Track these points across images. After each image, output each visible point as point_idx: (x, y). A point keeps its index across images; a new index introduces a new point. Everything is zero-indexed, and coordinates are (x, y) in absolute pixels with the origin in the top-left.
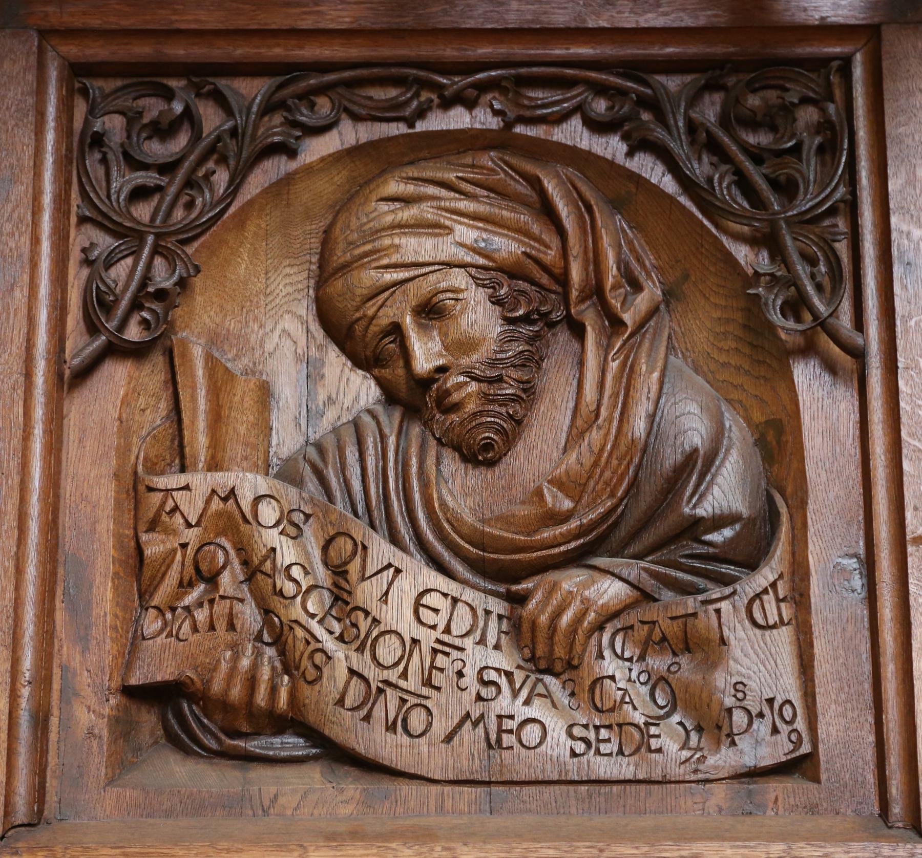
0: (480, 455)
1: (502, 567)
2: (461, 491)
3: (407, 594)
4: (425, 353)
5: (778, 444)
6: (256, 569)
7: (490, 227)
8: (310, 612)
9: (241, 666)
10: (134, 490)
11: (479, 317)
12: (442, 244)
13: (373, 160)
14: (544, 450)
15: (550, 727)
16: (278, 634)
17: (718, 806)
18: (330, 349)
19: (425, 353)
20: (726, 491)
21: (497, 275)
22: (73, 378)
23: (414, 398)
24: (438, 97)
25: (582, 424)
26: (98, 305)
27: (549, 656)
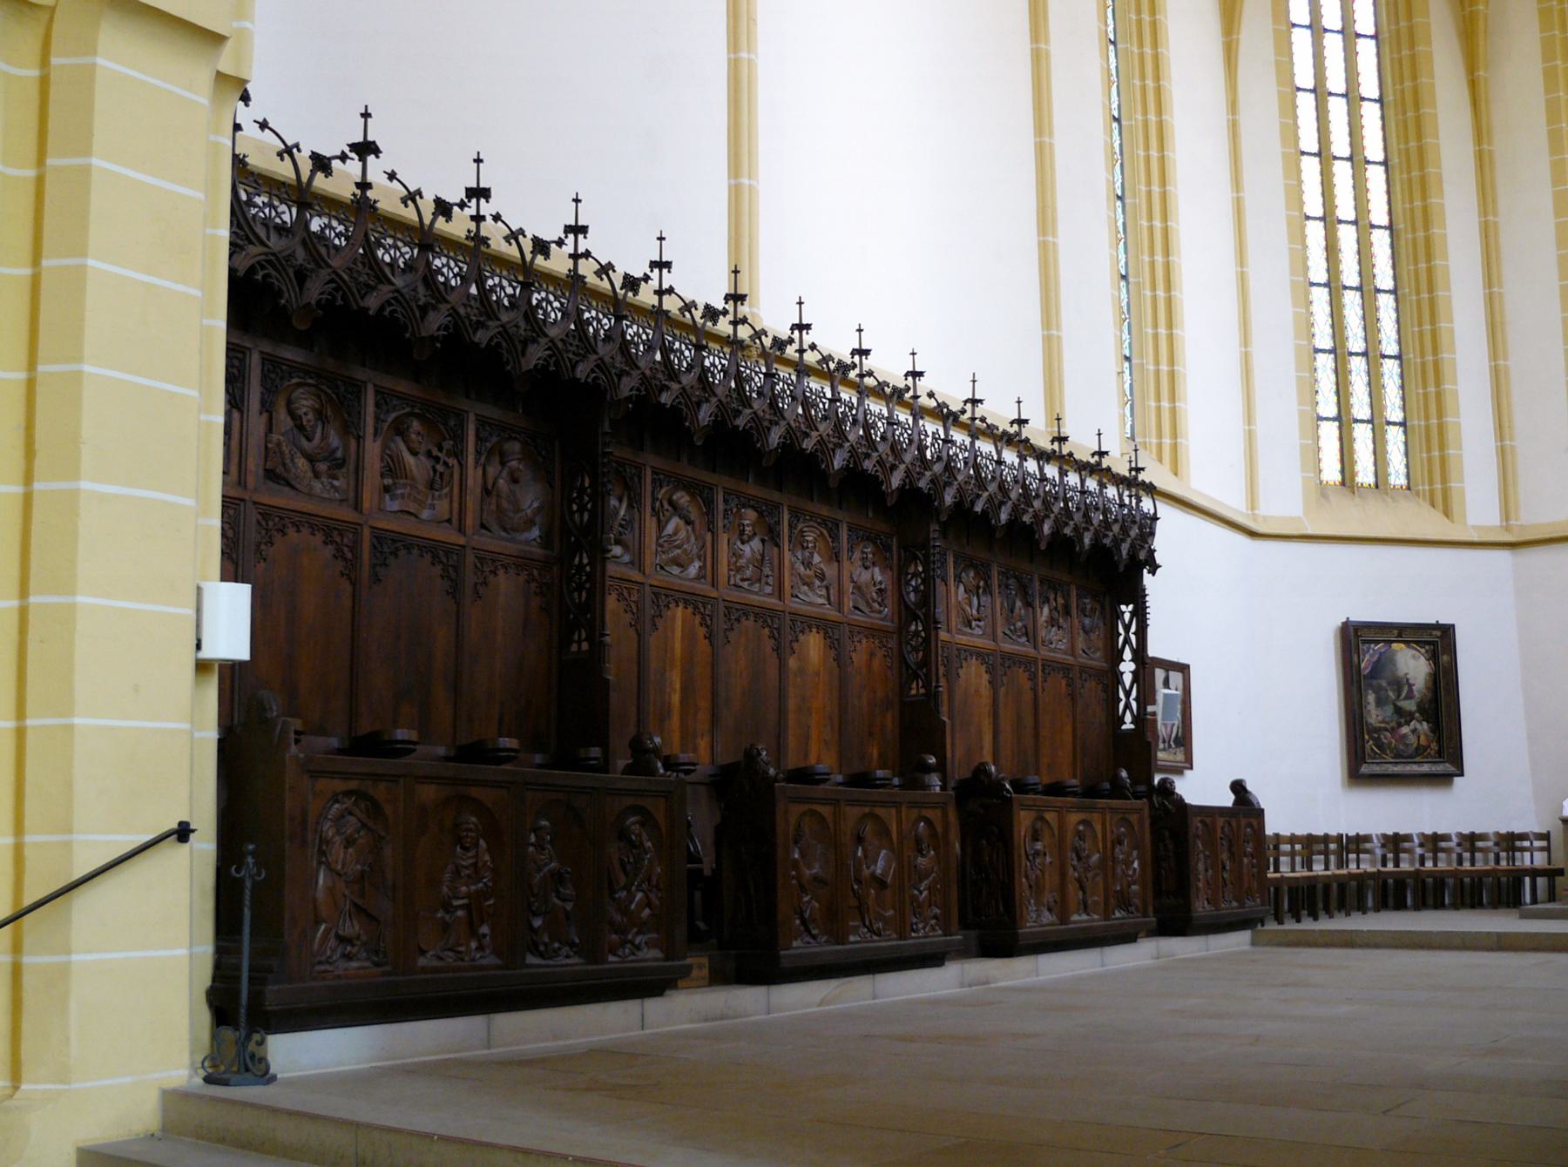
0: (309, 440)
1: (311, 459)
3: (301, 462)
5: (346, 447)
6: (282, 453)
9: (280, 470)
11: (310, 416)
13: (299, 385)
16: (284, 465)
20: (339, 454)
21: (314, 410)
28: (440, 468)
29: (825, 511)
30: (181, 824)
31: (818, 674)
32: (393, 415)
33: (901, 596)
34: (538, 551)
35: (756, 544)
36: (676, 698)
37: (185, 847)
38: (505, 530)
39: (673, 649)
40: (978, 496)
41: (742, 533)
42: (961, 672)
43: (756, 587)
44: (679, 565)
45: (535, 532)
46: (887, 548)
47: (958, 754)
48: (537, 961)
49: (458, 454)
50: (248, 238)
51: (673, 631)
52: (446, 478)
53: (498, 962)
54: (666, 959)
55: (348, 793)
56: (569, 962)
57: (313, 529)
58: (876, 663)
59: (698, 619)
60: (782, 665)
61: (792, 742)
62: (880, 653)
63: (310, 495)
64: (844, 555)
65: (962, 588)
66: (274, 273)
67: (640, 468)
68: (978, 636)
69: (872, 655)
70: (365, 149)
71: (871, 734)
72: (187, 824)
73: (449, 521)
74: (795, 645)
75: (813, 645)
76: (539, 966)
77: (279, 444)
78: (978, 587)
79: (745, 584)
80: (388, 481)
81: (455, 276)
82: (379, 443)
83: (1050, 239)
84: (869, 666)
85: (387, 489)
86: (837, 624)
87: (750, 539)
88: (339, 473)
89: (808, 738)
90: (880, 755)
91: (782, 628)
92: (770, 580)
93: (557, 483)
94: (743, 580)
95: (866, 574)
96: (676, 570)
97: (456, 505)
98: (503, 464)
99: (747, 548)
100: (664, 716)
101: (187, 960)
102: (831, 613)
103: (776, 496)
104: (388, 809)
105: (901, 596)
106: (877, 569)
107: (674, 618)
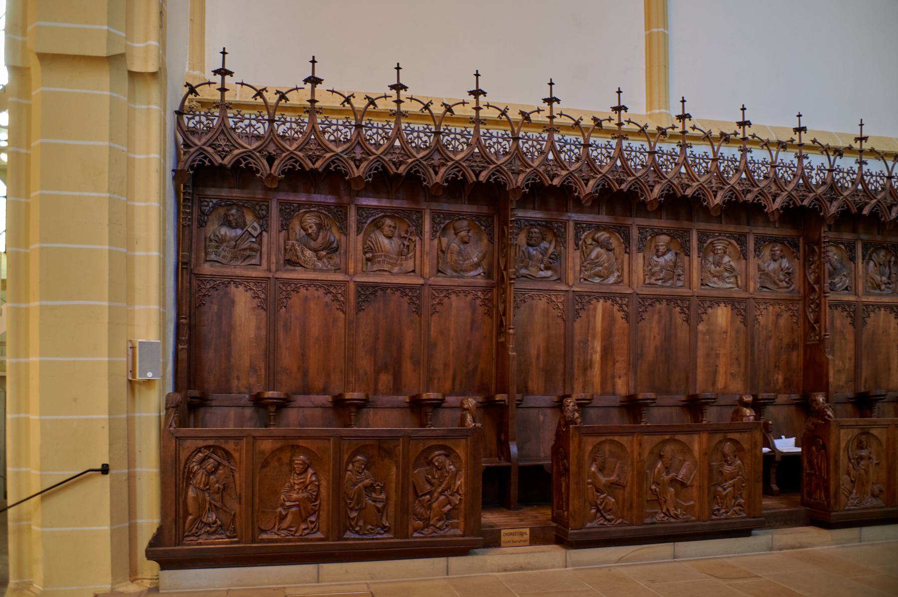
1: (315, 251)
2: (313, 244)
3: (309, 253)
4: (310, 231)
6: (296, 250)
7: (832, 467)
8: (299, 254)
9: (294, 258)
10: (285, 242)
11: (314, 227)
12: (311, 221)
13: (306, 212)
14: (320, 240)
15: (320, 264)
16: (297, 256)
17: (593, 396)
18: (536, 344)
19: (310, 231)
20: (335, 245)
21: (316, 224)
22: (280, 232)
23: (309, 235)
24: (222, 166)
25: (324, 238)
26: (282, 225)
27: (319, 259)
28: (406, 243)
29: (732, 228)
30: (103, 465)
31: (726, 332)
32: (371, 219)
33: (805, 276)
34: (481, 281)
35: (669, 257)
36: (597, 357)
37: (107, 477)
38: (456, 271)
39: (594, 328)
40: (866, 204)
41: (657, 251)
42: (869, 320)
43: (669, 283)
44: (600, 276)
45: (480, 270)
46: (796, 246)
47: (864, 375)
48: (353, 536)
49: (420, 233)
50: (233, 145)
51: (595, 317)
52: (411, 247)
53: (322, 536)
54: (285, 588)
55: (207, 447)
56: (387, 538)
57: (317, 287)
58: (782, 321)
59: (616, 307)
60: (693, 332)
61: (700, 376)
62: (786, 315)
63: (315, 269)
64: (751, 254)
65: (872, 264)
66: (252, 161)
67: (565, 224)
68: (887, 295)
69: (778, 315)
70: (314, 81)
71: (776, 366)
72: (107, 465)
73: (414, 271)
74: (704, 316)
75: (722, 315)
76: (354, 539)
77: (293, 245)
78: (890, 261)
79: (660, 283)
80: (369, 255)
81: (382, 138)
82: (360, 237)
83: (20, 38)
84: (776, 324)
85: (368, 260)
86: (741, 300)
87: (664, 254)
88: (334, 256)
89: (715, 372)
90: (785, 379)
91: (694, 308)
92: (682, 278)
93: (496, 240)
94: (657, 280)
95: (775, 263)
96: (597, 280)
97: (418, 262)
98: (456, 234)
99: (661, 260)
100: (587, 367)
101: (109, 532)
102: (738, 294)
103: (685, 224)
104: (236, 455)
105: (805, 276)
106: (785, 260)
107: (595, 309)
